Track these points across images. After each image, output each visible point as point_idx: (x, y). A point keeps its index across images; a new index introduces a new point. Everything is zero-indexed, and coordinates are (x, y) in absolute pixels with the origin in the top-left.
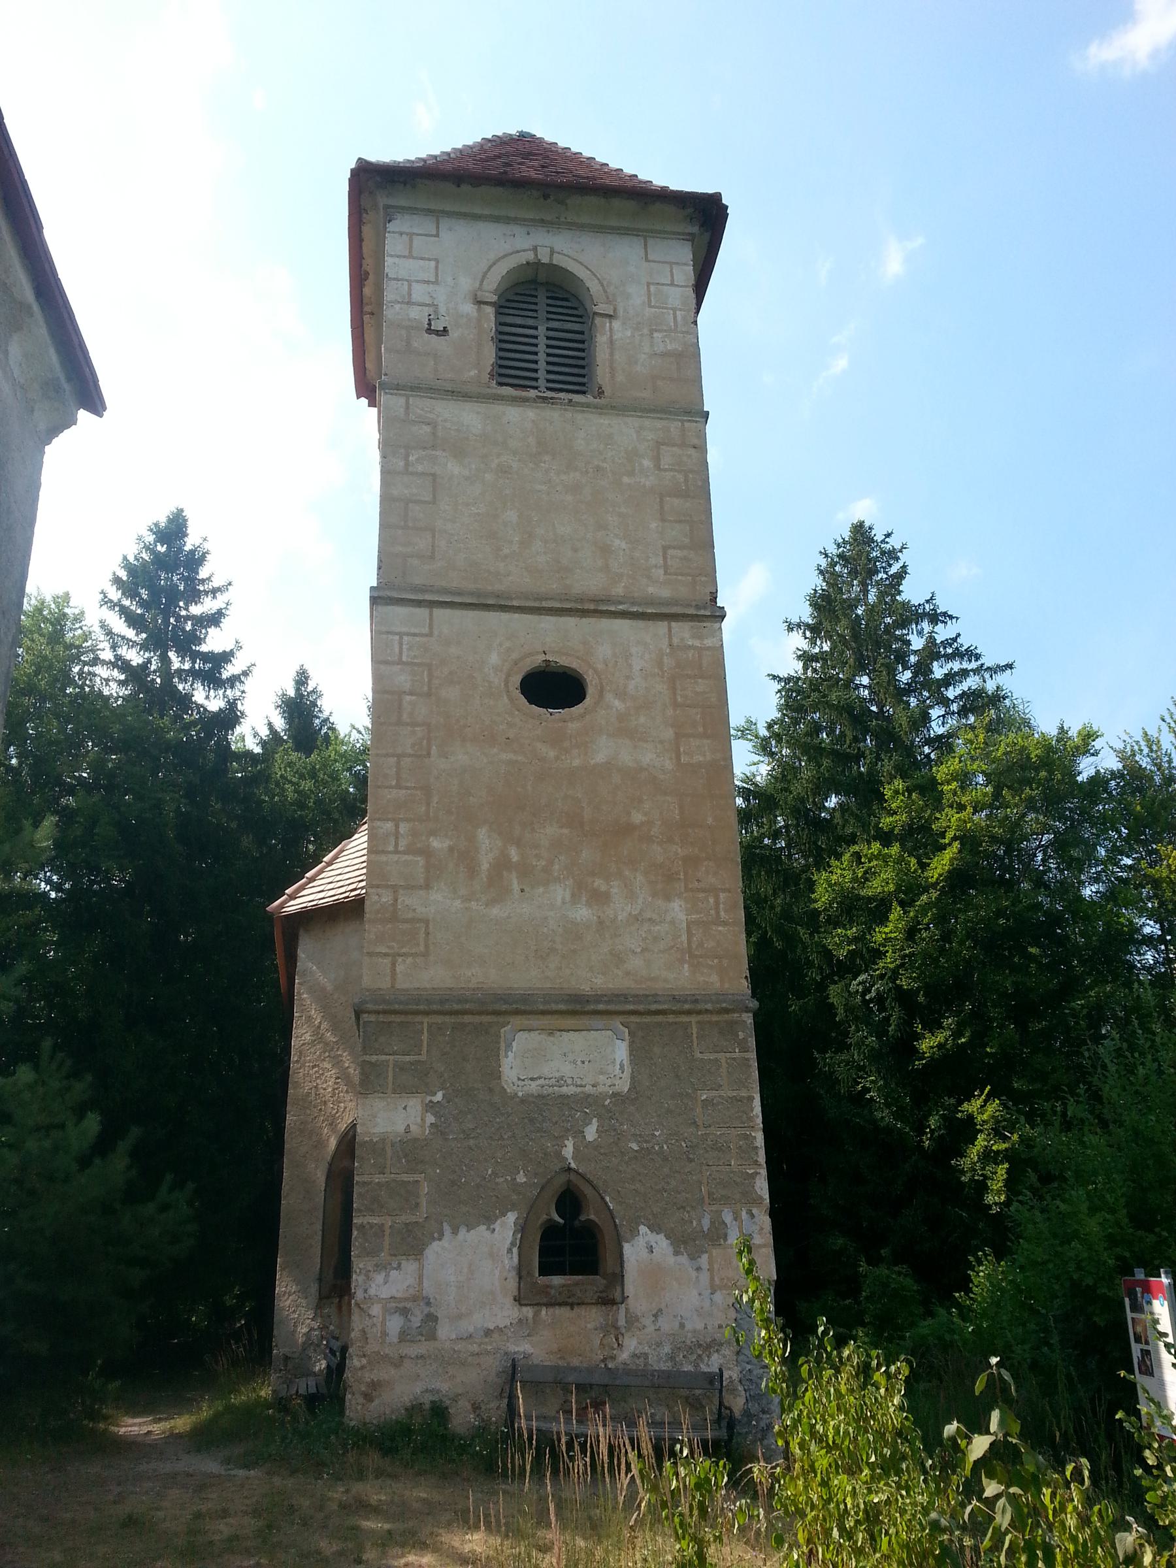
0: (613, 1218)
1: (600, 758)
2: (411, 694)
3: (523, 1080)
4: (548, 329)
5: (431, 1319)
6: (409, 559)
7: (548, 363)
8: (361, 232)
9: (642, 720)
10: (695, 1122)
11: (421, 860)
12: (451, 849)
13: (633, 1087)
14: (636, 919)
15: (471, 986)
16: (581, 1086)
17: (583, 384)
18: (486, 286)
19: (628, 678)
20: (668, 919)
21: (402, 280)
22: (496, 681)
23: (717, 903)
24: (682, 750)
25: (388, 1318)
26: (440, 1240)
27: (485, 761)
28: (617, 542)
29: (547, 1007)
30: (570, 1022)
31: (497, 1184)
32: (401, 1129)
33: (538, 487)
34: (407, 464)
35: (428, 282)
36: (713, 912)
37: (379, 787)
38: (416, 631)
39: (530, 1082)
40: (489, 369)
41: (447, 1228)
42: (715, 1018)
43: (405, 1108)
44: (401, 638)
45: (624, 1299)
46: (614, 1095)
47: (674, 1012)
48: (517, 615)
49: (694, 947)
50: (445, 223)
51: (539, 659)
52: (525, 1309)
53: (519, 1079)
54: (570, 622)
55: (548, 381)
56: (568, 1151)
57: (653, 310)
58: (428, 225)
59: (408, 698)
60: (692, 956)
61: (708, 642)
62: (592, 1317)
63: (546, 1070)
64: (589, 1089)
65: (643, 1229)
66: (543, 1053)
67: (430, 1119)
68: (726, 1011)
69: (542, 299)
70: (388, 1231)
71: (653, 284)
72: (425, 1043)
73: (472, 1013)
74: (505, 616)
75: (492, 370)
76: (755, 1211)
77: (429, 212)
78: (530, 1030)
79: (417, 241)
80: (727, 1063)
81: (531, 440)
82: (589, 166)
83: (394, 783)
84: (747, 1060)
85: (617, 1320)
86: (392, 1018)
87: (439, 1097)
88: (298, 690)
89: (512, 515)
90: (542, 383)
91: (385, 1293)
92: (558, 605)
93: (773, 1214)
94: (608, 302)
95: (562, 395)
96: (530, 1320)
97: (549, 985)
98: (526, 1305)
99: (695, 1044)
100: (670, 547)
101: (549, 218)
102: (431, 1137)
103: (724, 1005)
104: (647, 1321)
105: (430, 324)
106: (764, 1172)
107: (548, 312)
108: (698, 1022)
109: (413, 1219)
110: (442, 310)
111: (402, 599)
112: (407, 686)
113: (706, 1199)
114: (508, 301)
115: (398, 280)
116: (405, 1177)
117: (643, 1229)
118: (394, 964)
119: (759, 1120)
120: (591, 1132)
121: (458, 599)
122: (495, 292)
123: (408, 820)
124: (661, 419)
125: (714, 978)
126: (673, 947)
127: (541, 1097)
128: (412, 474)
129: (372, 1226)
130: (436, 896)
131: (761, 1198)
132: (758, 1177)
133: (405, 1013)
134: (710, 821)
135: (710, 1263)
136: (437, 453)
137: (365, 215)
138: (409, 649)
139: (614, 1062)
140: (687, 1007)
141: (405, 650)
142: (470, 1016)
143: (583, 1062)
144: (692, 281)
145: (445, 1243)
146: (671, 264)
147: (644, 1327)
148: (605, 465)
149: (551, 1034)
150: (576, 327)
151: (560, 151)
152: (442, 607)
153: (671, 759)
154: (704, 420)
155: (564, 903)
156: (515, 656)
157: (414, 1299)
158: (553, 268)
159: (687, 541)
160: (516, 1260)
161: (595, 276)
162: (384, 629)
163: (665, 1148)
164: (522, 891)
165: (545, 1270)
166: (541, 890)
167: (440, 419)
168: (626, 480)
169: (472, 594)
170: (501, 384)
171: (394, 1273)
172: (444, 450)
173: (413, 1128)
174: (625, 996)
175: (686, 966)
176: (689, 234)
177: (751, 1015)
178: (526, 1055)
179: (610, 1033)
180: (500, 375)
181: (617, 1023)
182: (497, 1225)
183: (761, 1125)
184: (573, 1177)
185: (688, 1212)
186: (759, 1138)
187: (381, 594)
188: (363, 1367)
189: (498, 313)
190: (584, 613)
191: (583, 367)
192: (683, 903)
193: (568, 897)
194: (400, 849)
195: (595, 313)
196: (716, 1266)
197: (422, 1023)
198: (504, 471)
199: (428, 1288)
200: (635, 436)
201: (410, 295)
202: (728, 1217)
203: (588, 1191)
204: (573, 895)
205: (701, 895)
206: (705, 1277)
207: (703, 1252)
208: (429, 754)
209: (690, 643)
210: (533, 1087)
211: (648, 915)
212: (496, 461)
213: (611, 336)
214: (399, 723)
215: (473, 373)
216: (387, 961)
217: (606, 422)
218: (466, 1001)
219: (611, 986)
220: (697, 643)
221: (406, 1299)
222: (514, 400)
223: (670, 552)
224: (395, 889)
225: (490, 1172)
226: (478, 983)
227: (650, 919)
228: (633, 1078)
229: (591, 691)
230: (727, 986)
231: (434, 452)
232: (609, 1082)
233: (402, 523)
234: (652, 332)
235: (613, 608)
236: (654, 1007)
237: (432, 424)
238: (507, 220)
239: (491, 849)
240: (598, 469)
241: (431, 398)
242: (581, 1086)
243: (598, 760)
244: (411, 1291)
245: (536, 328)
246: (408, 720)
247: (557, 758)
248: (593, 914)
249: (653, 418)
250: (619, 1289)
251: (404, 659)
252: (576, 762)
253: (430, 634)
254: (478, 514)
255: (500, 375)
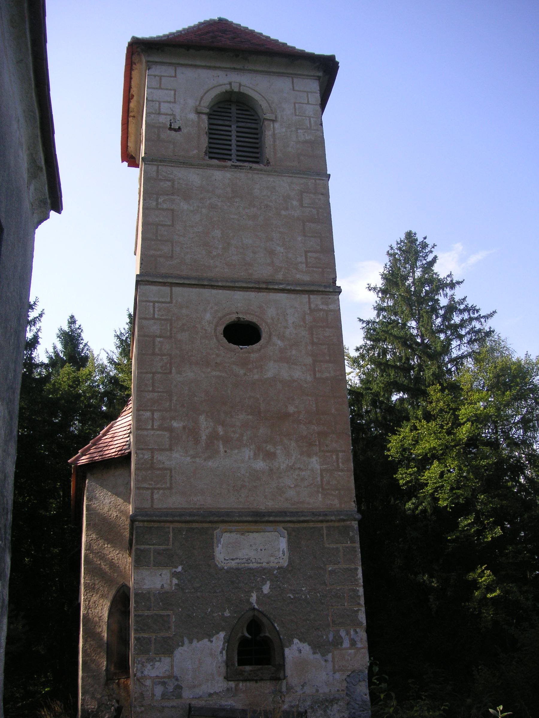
0: (279, 635)
1: (270, 374)
2: (160, 337)
3: (228, 560)
4: (237, 127)
5: (179, 687)
6: (158, 259)
7: (237, 146)
8: (131, 74)
9: (294, 352)
10: (325, 583)
11: (167, 434)
12: (184, 427)
13: (290, 564)
14: (291, 468)
15: (197, 507)
16: (260, 563)
17: (257, 158)
18: (202, 104)
19: (286, 327)
20: (310, 467)
21: (156, 101)
22: (209, 329)
23: (337, 459)
24: (317, 369)
25: (155, 687)
26: (182, 646)
27: (203, 376)
28: (278, 248)
29: (241, 519)
30: (253, 527)
31: (213, 617)
32: (159, 586)
33: (232, 217)
34: (157, 204)
35: (170, 102)
36: (335, 464)
37: (142, 391)
38: (163, 300)
39: (231, 561)
40: (204, 150)
41: (186, 641)
42: (336, 524)
43: (161, 575)
44: (154, 304)
45: (285, 677)
46: (279, 568)
47: (313, 521)
48: (221, 291)
49: (324, 484)
50: (180, 70)
51: (234, 317)
52: (230, 683)
53: (225, 559)
54: (252, 295)
55: (238, 156)
56: (254, 598)
57: (297, 117)
58: (170, 71)
59: (158, 339)
60: (323, 489)
61: (332, 307)
62: (267, 687)
63: (240, 555)
64: (264, 565)
65: (296, 641)
66: (238, 545)
67: (175, 581)
68: (343, 520)
69: (234, 109)
70: (153, 641)
71: (297, 103)
72: (171, 539)
73: (198, 522)
74: (214, 291)
75: (206, 151)
76: (358, 630)
77: (171, 64)
78: (231, 532)
79: (164, 80)
80: (344, 550)
81: (229, 190)
82: (259, 38)
83: (151, 389)
84: (355, 547)
85: (281, 688)
86: (152, 524)
87: (180, 569)
88: (70, 327)
89: (217, 233)
90: (234, 157)
91: (153, 674)
92: (245, 285)
93: (367, 631)
94: (272, 113)
95: (246, 164)
96: (234, 689)
97: (241, 507)
98: (231, 681)
99: (325, 539)
100: (309, 252)
101: (238, 67)
102: (176, 591)
103: (342, 517)
104: (298, 689)
105: (171, 125)
106: (363, 609)
107: (237, 118)
108: (326, 527)
109: (167, 635)
110: (178, 118)
111: (155, 282)
112: (158, 333)
113: (331, 624)
114: (214, 111)
115: (153, 101)
116: (162, 613)
117: (296, 641)
118: (152, 494)
119: (361, 581)
120: (266, 589)
121: (187, 282)
122: (207, 107)
123: (159, 411)
124: (303, 178)
125: (336, 502)
126: (311, 484)
127: (238, 569)
128: (160, 209)
129: (144, 638)
130: (175, 455)
131: (361, 623)
132: (360, 612)
133: (159, 522)
134: (333, 411)
135: (333, 658)
136: (175, 197)
137: (134, 66)
138: (158, 311)
139: (279, 549)
140: (321, 518)
141: (156, 311)
142: (197, 524)
143: (261, 550)
144: (319, 102)
145: (185, 648)
146: (307, 92)
147: (296, 692)
148: (271, 204)
149: (242, 534)
150: (253, 126)
151: (242, 29)
152: (178, 286)
153: (310, 375)
154: (328, 179)
155: (249, 458)
156: (220, 315)
157: (169, 677)
158: (240, 94)
159: (319, 247)
160: (225, 657)
161: (264, 98)
162: (144, 299)
163: (308, 596)
164: (226, 452)
165: (241, 663)
166: (236, 451)
167: (176, 178)
168: (283, 213)
169: (195, 278)
170: (211, 158)
171: (157, 664)
172: (178, 196)
173: (165, 586)
174: (285, 513)
175: (320, 495)
176: (318, 76)
177: (357, 522)
178: (229, 546)
179: (276, 533)
180: (210, 153)
181: (280, 527)
182: (214, 639)
183: (362, 584)
184: (256, 613)
185: (321, 631)
186: (361, 591)
187: (143, 278)
188: (142, 712)
189: (209, 118)
190: (259, 290)
191: (257, 134)
192: (318, 459)
193: (252, 454)
194: (155, 427)
195: (265, 119)
196: (336, 660)
197: (169, 528)
198: (212, 207)
199: (176, 672)
200: (288, 188)
201: (160, 109)
202: (343, 633)
203: (264, 620)
204: (255, 454)
205: (328, 454)
206: (330, 666)
207: (329, 652)
208: (170, 373)
209: (321, 307)
210: (233, 564)
211: (298, 466)
212: (208, 202)
213: (274, 132)
214: (154, 354)
215: (195, 152)
216: (149, 492)
217: (272, 179)
218: (194, 515)
219: (277, 506)
220: (325, 307)
221: (164, 677)
222: (218, 167)
223: (309, 254)
224: (152, 451)
225: (209, 610)
226: (201, 505)
227: (299, 468)
228: (290, 558)
229: (264, 335)
230: (343, 506)
231: (173, 197)
232: (276, 561)
233: (154, 238)
234: (297, 129)
235: (276, 287)
236: (302, 518)
237: (172, 181)
238: (215, 68)
239: (207, 427)
240: (267, 206)
241: (172, 166)
242: (260, 563)
243: (268, 376)
244: (167, 673)
245: (230, 126)
246: (158, 352)
247: (245, 374)
248: (267, 465)
249: (299, 177)
250: (282, 672)
251: (156, 316)
252: (256, 377)
253: (171, 302)
254: (199, 232)
255: (210, 153)
